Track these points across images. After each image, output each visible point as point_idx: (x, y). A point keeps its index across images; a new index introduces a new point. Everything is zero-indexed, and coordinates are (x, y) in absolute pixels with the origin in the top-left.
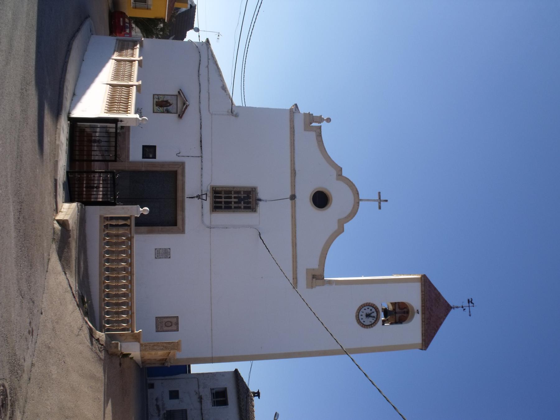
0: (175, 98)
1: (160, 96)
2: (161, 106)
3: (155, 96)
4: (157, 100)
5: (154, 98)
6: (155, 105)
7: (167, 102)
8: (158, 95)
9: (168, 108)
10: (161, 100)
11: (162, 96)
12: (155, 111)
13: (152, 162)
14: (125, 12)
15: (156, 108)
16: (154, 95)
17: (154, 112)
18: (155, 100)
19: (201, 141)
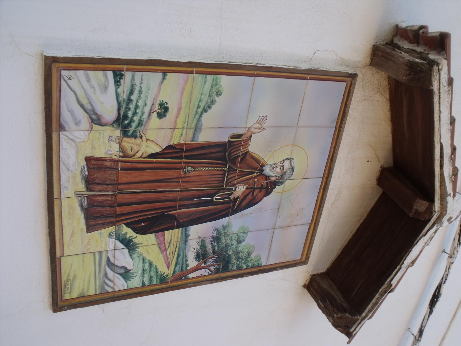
0: (322, 100)
1: (152, 89)
2: (155, 221)
3: (77, 86)
4: (106, 145)
5: (52, 123)
6: (73, 218)
7: (231, 156)
8: (118, 68)
9: (235, 223)
10: (156, 137)
11: (170, 90)
12: (81, 277)
13: (187, 211)
14: (376, 186)
15: (92, 250)
16: (53, 69)
17: (59, 303)
18: (81, 144)
19: (444, 338)
